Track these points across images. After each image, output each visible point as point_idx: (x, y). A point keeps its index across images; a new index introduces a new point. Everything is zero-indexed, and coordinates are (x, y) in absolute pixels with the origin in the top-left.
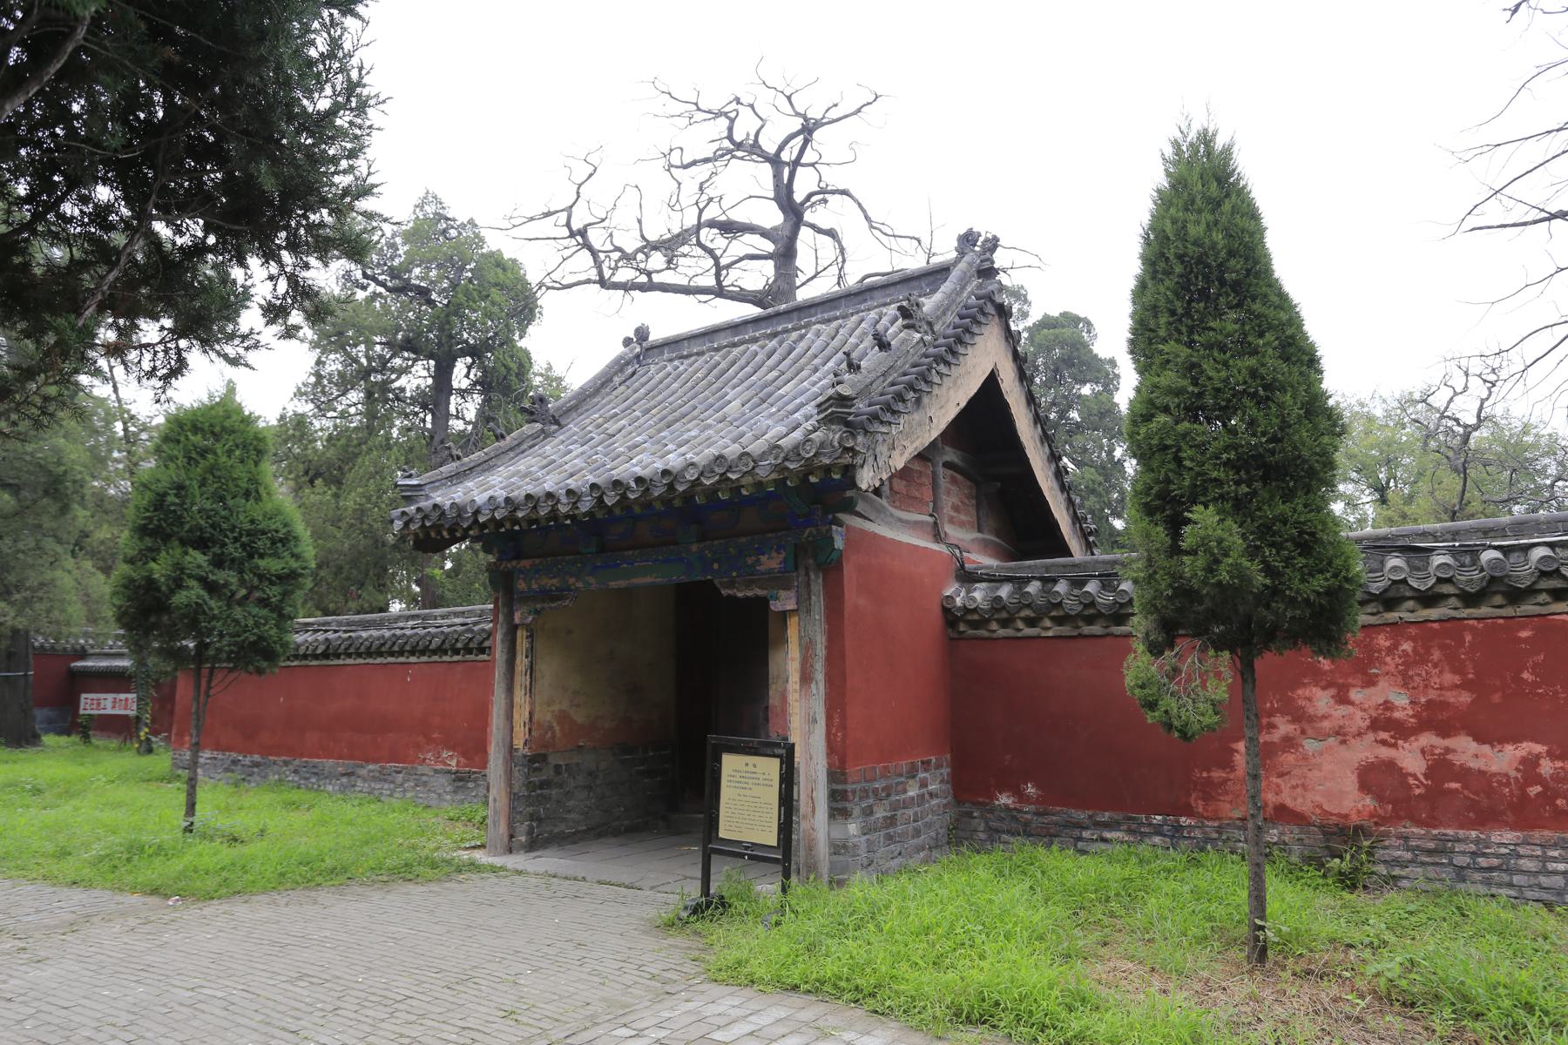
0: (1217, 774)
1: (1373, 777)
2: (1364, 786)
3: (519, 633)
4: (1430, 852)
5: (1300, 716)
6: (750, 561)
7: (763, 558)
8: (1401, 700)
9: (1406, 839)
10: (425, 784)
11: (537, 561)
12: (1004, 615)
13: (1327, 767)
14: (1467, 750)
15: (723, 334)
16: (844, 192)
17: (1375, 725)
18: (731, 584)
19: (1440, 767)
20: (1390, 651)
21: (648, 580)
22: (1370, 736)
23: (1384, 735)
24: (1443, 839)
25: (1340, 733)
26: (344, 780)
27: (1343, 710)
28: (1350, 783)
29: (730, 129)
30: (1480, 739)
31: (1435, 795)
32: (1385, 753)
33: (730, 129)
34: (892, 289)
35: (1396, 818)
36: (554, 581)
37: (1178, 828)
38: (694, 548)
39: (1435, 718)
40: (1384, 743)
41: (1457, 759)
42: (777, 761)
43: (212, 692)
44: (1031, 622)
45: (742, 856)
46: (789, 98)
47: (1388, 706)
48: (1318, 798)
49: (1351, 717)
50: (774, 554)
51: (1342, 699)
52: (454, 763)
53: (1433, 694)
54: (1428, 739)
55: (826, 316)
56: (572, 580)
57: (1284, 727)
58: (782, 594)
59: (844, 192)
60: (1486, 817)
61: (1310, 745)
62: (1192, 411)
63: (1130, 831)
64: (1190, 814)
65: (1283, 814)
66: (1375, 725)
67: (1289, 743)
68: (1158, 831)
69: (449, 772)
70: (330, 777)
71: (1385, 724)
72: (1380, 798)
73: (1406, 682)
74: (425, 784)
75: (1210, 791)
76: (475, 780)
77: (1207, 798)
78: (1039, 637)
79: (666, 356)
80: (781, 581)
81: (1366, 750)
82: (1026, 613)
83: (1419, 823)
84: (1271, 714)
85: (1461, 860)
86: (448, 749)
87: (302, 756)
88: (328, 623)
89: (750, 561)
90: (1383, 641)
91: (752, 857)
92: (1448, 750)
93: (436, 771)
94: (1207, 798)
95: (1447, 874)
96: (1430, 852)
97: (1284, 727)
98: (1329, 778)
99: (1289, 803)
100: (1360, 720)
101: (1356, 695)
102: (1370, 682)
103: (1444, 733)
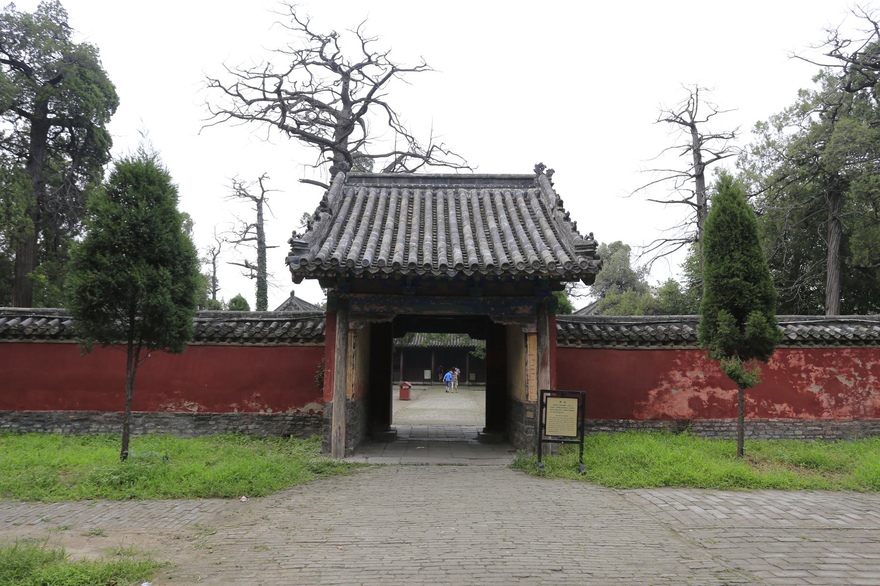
0: (643, 403)
1: (694, 402)
2: (690, 406)
3: (349, 334)
4: (708, 427)
5: (671, 382)
6: (512, 308)
7: (520, 308)
8: (702, 376)
9: (701, 423)
10: (166, 424)
11: (370, 296)
12: (562, 337)
13: (679, 399)
14: (720, 393)
15: (403, 180)
16: (384, 104)
17: (694, 384)
18: (500, 318)
19: (712, 398)
20: (699, 358)
21: (449, 312)
22: (692, 388)
23: (696, 388)
24: (712, 422)
25: (683, 387)
26: (77, 424)
27: (684, 379)
28: (686, 404)
29: (322, 48)
30: (723, 389)
31: (710, 407)
32: (696, 394)
33: (322, 48)
34: (503, 181)
35: (698, 416)
36: (382, 307)
37: (628, 424)
38: (481, 299)
39: (711, 382)
40: (696, 390)
41: (716, 395)
42: (576, 400)
43: (139, 364)
44: (571, 341)
45: (560, 442)
46: (363, 44)
47: (698, 378)
48: (676, 410)
49: (686, 381)
50: (526, 306)
51: (684, 375)
52: (195, 409)
53: (711, 374)
54: (709, 389)
55: (468, 185)
56: (395, 308)
57: (666, 385)
58: (529, 325)
59: (384, 104)
60: (723, 414)
61: (674, 391)
62: (746, 279)
63: (610, 426)
64: (633, 419)
65: (665, 417)
66: (694, 384)
67: (667, 391)
68: (621, 425)
69: (191, 415)
70: (59, 423)
71: (697, 384)
72: (694, 409)
73: (703, 370)
74: (166, 424)
75: (640, 409)
76: (215, 420)
77: (639, 412)
78: (575, 348)
79: (364, 183)
80: (527, 319)
81: (690, 393)
82: (571, 337)
83: (705, 418)
84: (661, 380)
85: (717, 429)
86: (189, 400)
87: (23, 408)
88: (50, 313)
89: (512, 308)
90: (697, 355)
91: (565, 442)
92: (714, 392)
93: (177, 415)
94: (639, 412)
95: (712, 433)
96: (708, 427)
97: (666, 385)
98: (679, 404)
99: (667, 412)
100: (689, 382)
101: (688, 374)
102: (693, 369)
103: (713, 387)
